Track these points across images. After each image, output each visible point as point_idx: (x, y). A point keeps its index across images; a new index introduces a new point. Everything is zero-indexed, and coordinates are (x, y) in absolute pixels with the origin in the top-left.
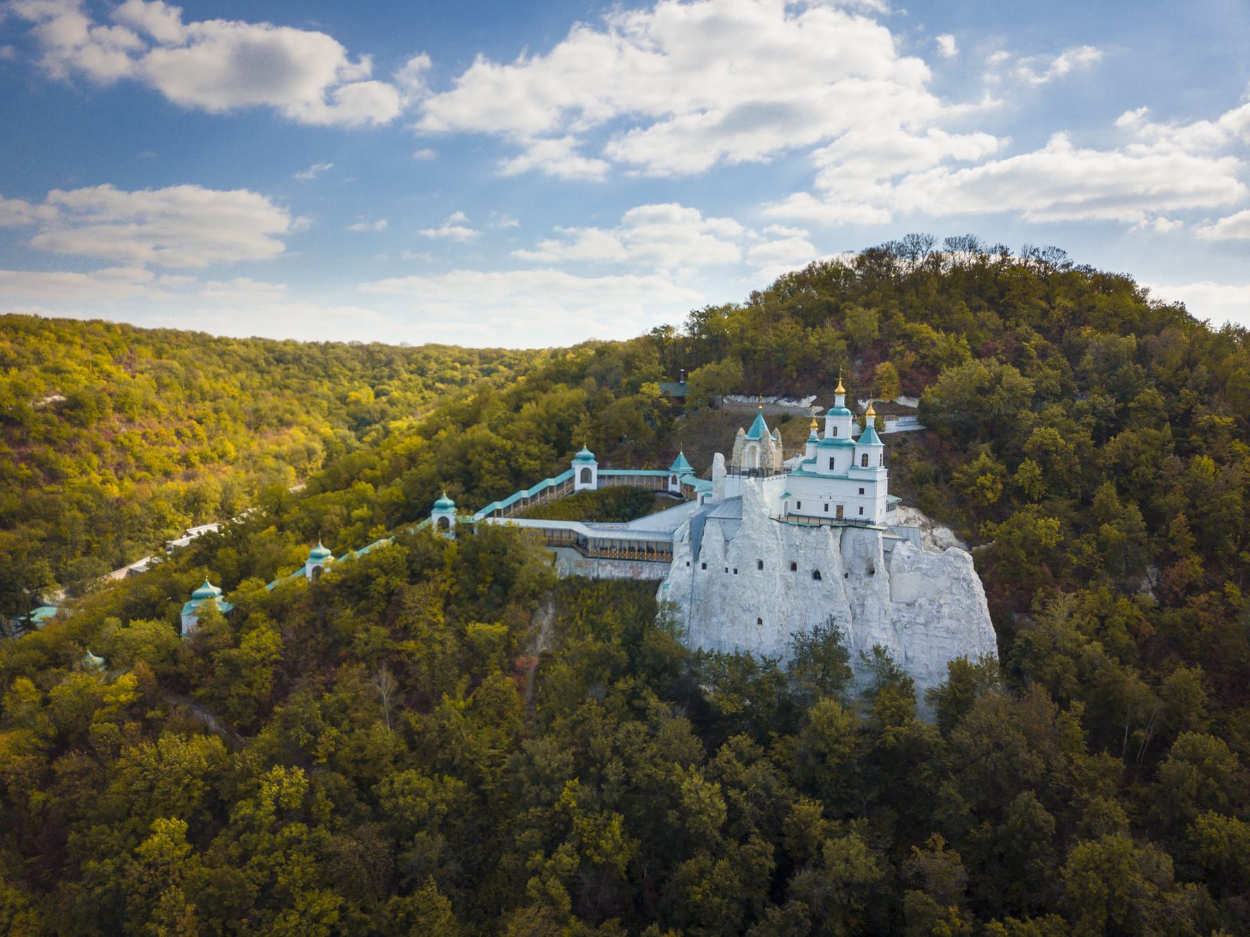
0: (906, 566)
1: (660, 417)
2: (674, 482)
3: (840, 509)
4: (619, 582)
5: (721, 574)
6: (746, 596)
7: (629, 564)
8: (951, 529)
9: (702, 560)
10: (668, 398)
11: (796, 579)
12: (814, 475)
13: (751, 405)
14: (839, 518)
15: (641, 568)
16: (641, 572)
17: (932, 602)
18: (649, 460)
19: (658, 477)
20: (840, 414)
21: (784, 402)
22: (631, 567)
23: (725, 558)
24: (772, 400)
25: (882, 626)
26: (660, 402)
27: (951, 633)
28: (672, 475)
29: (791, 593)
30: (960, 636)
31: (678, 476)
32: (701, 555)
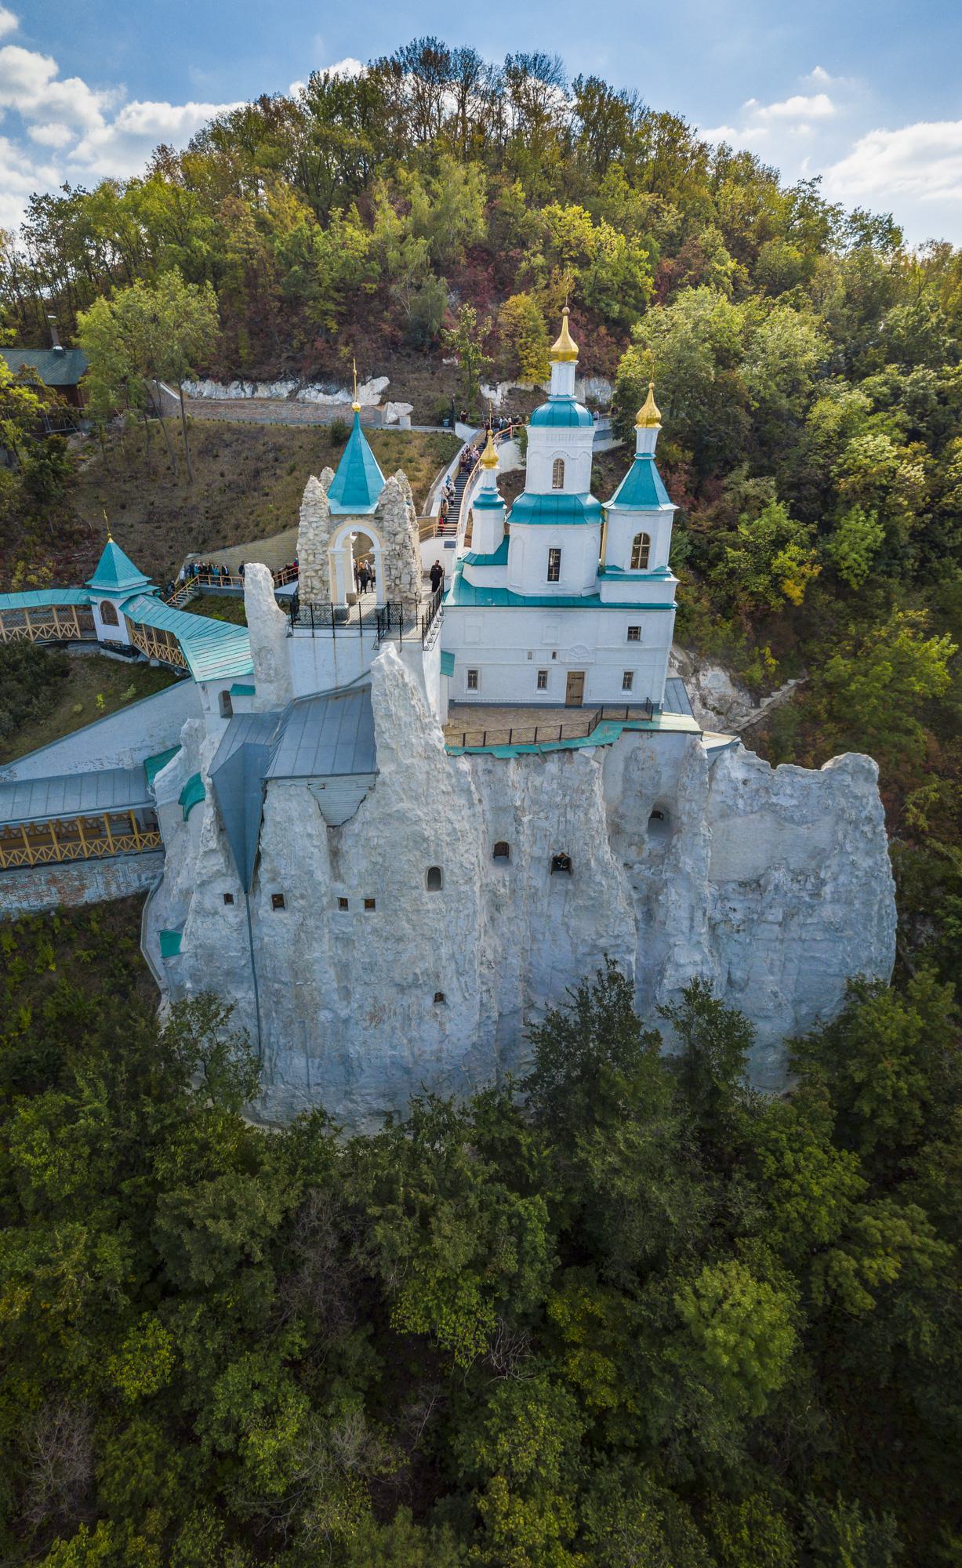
0: (740, 802)
1: (26, 442)
2: (110, 618)
3: (576, 679)
4: (26, 924)
5: (329, 913)
6: (405, 958)
7: (41, 875)
8: (725, 667)
9: (267, 889)
10: (35, 388)
11: (514, 880)
12: (502, 598)
13: (238, 403)
14: (574, 702)
15: (81, 878)
16: (83, 887)
17: (798, 875)
18: (24, 557)
19: (62, 609)
20: (572, 420)
21: (314, 395)
22: (53, 881)
23: (337, 876)
24: (283, 389)
25: (695, 938)
26: (17, 400)
27: (833, 930)
28: (99, 600)
29: (507, 913)
30: (849, 932)
31: (117, 604)
32: (264, 875)
